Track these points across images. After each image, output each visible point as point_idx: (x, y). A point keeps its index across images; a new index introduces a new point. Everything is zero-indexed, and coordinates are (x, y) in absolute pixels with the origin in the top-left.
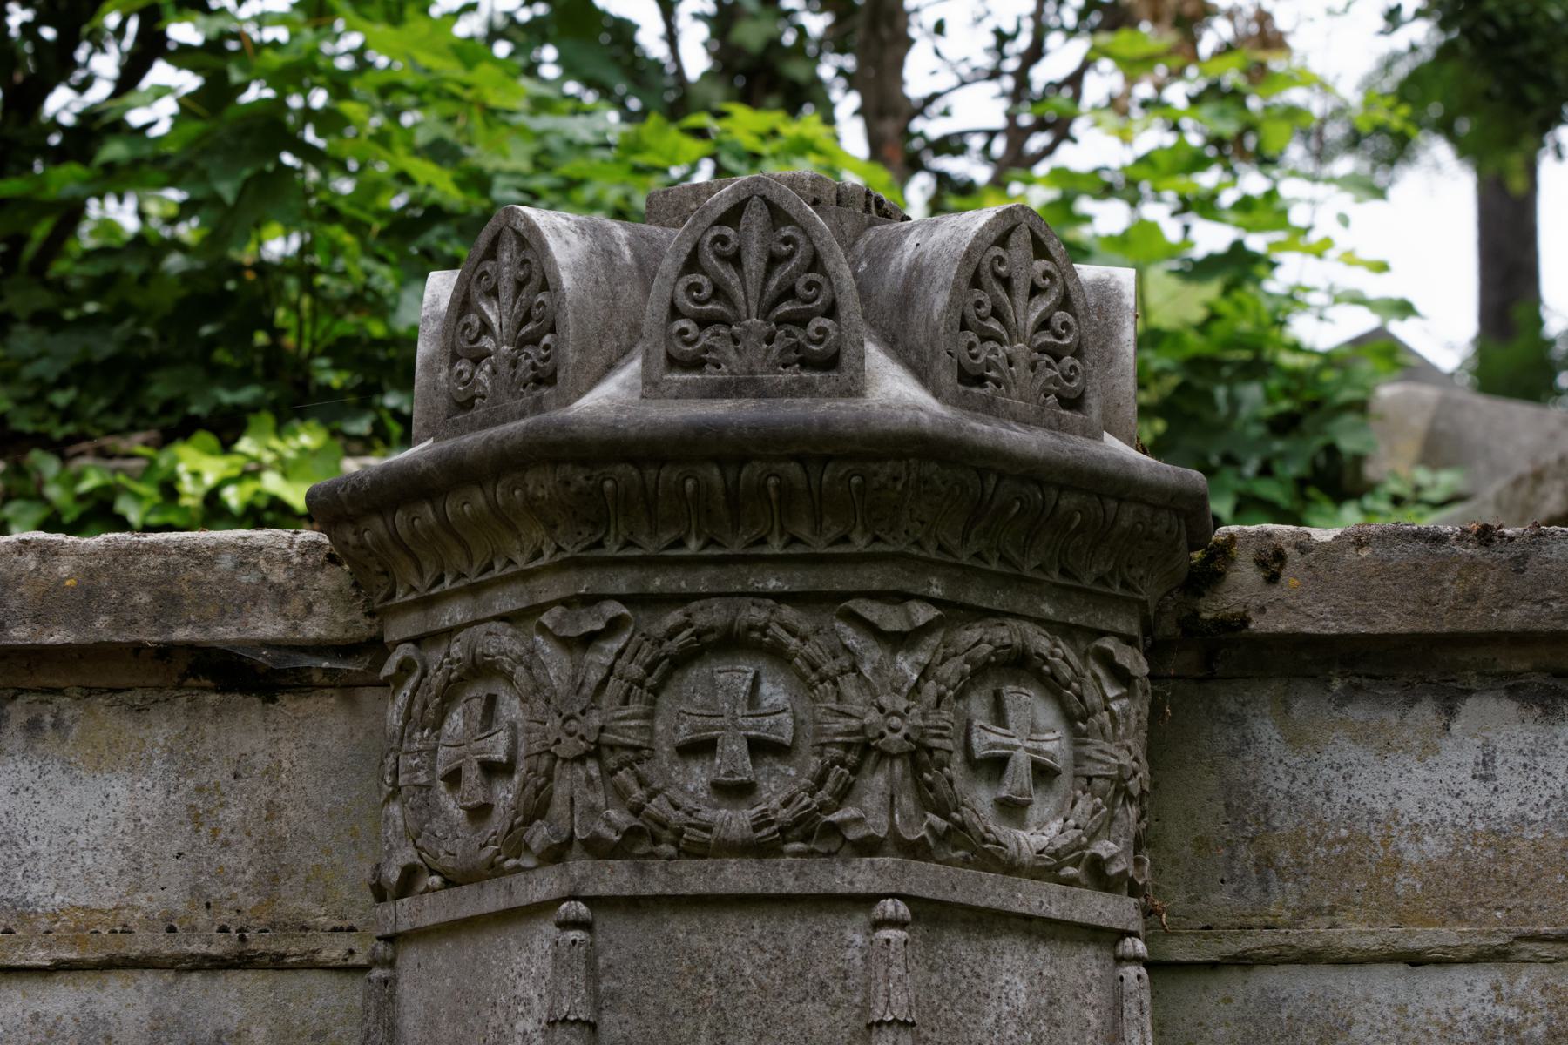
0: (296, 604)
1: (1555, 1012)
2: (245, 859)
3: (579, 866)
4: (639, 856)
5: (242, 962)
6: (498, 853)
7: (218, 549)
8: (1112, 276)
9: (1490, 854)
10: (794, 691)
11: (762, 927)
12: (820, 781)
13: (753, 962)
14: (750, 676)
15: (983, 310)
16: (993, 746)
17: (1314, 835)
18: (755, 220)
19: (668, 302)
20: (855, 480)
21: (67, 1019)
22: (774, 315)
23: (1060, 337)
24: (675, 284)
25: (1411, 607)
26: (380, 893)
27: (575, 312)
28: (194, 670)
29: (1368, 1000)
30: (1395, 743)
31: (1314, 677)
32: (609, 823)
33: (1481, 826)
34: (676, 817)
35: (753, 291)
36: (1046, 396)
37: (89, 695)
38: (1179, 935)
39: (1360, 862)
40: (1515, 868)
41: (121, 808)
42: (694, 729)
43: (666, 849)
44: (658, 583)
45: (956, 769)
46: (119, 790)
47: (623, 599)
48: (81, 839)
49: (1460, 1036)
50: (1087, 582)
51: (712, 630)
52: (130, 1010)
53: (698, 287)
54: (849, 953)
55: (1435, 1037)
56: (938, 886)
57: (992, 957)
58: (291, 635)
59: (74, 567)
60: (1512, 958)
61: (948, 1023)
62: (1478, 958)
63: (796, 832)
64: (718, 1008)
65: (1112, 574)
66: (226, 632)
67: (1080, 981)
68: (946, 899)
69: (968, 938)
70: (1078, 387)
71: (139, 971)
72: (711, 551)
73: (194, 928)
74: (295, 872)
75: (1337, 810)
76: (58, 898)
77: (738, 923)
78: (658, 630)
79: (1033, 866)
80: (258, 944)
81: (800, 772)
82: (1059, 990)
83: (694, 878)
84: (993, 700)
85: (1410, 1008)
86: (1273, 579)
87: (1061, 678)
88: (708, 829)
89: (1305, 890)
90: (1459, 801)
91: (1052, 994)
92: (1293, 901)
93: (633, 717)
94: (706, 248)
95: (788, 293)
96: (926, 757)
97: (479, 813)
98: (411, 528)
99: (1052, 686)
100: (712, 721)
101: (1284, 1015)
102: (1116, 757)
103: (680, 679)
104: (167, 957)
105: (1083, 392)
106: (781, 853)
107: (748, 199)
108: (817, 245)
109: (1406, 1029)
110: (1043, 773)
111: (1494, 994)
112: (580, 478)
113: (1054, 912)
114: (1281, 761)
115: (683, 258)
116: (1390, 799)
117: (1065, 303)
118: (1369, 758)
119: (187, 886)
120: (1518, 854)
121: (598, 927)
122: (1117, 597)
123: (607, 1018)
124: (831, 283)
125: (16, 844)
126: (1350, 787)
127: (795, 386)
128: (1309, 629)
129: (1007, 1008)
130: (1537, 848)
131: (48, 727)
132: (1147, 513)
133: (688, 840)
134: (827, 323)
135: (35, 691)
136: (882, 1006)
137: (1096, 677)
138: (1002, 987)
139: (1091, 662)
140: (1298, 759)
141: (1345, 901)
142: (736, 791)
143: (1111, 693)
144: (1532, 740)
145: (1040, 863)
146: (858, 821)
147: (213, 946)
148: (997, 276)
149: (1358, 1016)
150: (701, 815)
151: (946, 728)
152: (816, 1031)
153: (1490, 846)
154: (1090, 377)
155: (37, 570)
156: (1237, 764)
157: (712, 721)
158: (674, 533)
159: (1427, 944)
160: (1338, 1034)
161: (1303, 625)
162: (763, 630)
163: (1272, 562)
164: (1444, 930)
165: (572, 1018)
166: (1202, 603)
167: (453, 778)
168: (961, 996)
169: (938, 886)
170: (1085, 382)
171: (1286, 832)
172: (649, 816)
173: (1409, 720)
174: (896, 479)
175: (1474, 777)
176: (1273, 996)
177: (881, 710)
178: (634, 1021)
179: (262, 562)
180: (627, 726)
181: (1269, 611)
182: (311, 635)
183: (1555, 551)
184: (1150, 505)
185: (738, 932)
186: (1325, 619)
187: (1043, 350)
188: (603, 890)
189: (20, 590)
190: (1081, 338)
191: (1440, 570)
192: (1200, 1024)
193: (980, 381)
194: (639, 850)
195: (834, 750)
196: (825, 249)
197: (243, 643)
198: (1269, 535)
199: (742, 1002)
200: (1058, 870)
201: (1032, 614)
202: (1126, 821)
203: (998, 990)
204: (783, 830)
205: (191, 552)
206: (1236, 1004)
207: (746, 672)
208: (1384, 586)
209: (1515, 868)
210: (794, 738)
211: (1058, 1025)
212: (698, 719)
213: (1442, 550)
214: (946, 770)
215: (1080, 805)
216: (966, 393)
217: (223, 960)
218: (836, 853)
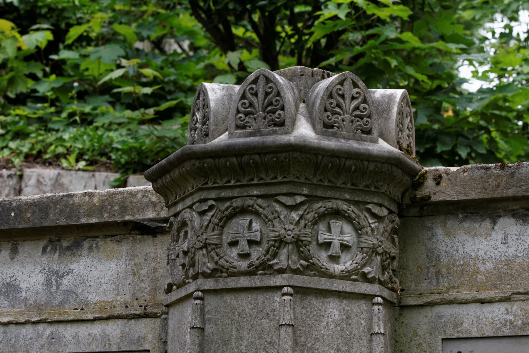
0: (159, 207)
1: (524, 317)
2: (147, 285)
3: (200, 281)
4: (217, 277)
5: (145, 316)
6: (184, 278)
7: (137, 192)
8: (395, 92)
9: (506, 267)
10: (262, 225)
11: (251, 297)
12: (267, 252)
13: (248, 308)
14: (248, 221)
15: (333, 105)
16: (325, 239)
17: (453, 264)
18: (261, 82)
19: (236, 108)
20: (274, 159)
21: (98, 334)
22: (266, 111)
23: (363, 112)
24: (238, 103)
25: (479, 190)
27: (214, 114)
28: (133, 229)
29: (468, 315)
30: (478, 233)
31: (454, 214)
32: (207, 267)
33: (503, 259)
34: (226, 265)
35: (260, 104)
36: (357, 131)
37: (106, 238)
38: (411, 297)
39: (467, 272)
40: (514, 271)
41: (114, 271)
42: (233, 238)
43: (225, 274)
44: (223, 194)
46: (113, 265)
47: (214, 199)
48: (103, 281)
49: (495, 325)
50: (361, 187)
51: (238, 207)
52: (115, 331)
53: (245, 104)
54: (275, 304)
55: (488, 326)
56: (304, 282)
57: (326, 304)
58: (157, 217)
59: (98, 200)
60: (512, 300)
61: (309, 325)
62: (501, 300)
63: (261, 268)
64: (238, 322)
65: (371, 184)
66: (139, 217)
67: (359, 311)
68: (307, 286)
69: (317, 298)
70: (369, 127)
71: (118, 320)
72: (239, 183)
73: (133, 306)
74: (161, 288)
75: (460, 256)
76: (96, 298)
77: (244, 296)
78: (223, 208)
79: (340, 276)
80: (149, 310)
81: (263, 249)
82: (351, 314)
83: (232, 283)
84: (328, 225)
85: (481, 317)
86: (438, 184)
87: (351, 217)
88: (235, 268)
89: (450, 281)
90: (497, 251)
91: (348, 315)
92: (446, 285)
93: (215, 235)
94: (247, 92)
95: (271, 104)
96: (300, 243)
98: (166, 182)
99: (349, 220)
100: (237, 235)
101: (443, 321)
102: (372, 241)
103: (230, 223)
104: (125, 315)
105: (371, 129)
106: (256, 274)
107: (259, 76)
108: (279, 88)
109: (479, 324)
110: (345, 247)
111: (506, 312)
112: (197, 163)
113: (348, 290)
114: (443, 241)
115: (241, 95)
116: (476, 251)
117: (365, 101)
118: (470, 239)
119: (131, 294)
120: (514, 267)
121: (205, 299)
122: (372, 192)
123: (207, 326)
124: (282, 100)
125: (85, 283)
126: (464, 248)
127: (271, 132)
128: (449, 199)
129: (331, 320)
130: (520, 265)
131: (94, 248)
132: (379, 165)
133: (230, 272)
134: (281, 112)
135: (91, 237)
136: (282, 319)
137: (365, 217)
138: (329, 313)
139: (364, 212)
140: (448, 240)
141: (462, 284)
142: (244, 256)
143: (371, 221)
144: (519, 231)
145: (342, 275)
146: (277, 263)
147: (137, 311)
148: (339, 94)
149: (465, 320)
150: (233, 264)
151: (307, 234)
152: (265, 328)
153: (506, 265)
154: (374, 124)
155: (88, 201)
156: (430, 242)
157: (237, 235)
158: (227, 179)
159: (485, 296)
160: (459, 326)
161: (447, 198)
162: (252, 206)
163: (438, 179)
164: (491, 292)
165: (195, 326)
166: (417, 192)
168: (314, 316)
169: (304, 282)
170: (372, 125)
171: (445, 263)
172: (219, 265)
173: (482, 226)
174: (286, 158)
175: (501, 243)
176: (440, 315)
177: (285, 229)
178: (215, 327)
179: (149, 195)
180: (212, 236)
181: (437, 194)
182: (163, 216)
183: (523, 170)
184: (380, 162)
185: (245, 299)
186: (453, 196)
187: (356, 116)
188: (206, 288)
189: (83, 207)
190: (370, 112)
191: (489, 178)
192: (418, 324)
193: (332, 127)
194: (217, 275)
195: (271, 242)
196: (281, 89)
197: (144, 220)
198: (437, 170)
199: (245, 320)
200: (350, 277)
201: (341, 198)
202: (376, 261)
203: (328, 314)
204: (256, 267)
205: (130, 193)
206: (429, 317)
207: (247, 220)
208: (472, 184)
209: (514, 271)
210: (261, 239)
211: (350, 325)
212: (233, 235)
213: (489, 172)
214: (307, 247)
215: (358, 256)
216: (325, 131)
217: (140, 315)
218: (273, 274)
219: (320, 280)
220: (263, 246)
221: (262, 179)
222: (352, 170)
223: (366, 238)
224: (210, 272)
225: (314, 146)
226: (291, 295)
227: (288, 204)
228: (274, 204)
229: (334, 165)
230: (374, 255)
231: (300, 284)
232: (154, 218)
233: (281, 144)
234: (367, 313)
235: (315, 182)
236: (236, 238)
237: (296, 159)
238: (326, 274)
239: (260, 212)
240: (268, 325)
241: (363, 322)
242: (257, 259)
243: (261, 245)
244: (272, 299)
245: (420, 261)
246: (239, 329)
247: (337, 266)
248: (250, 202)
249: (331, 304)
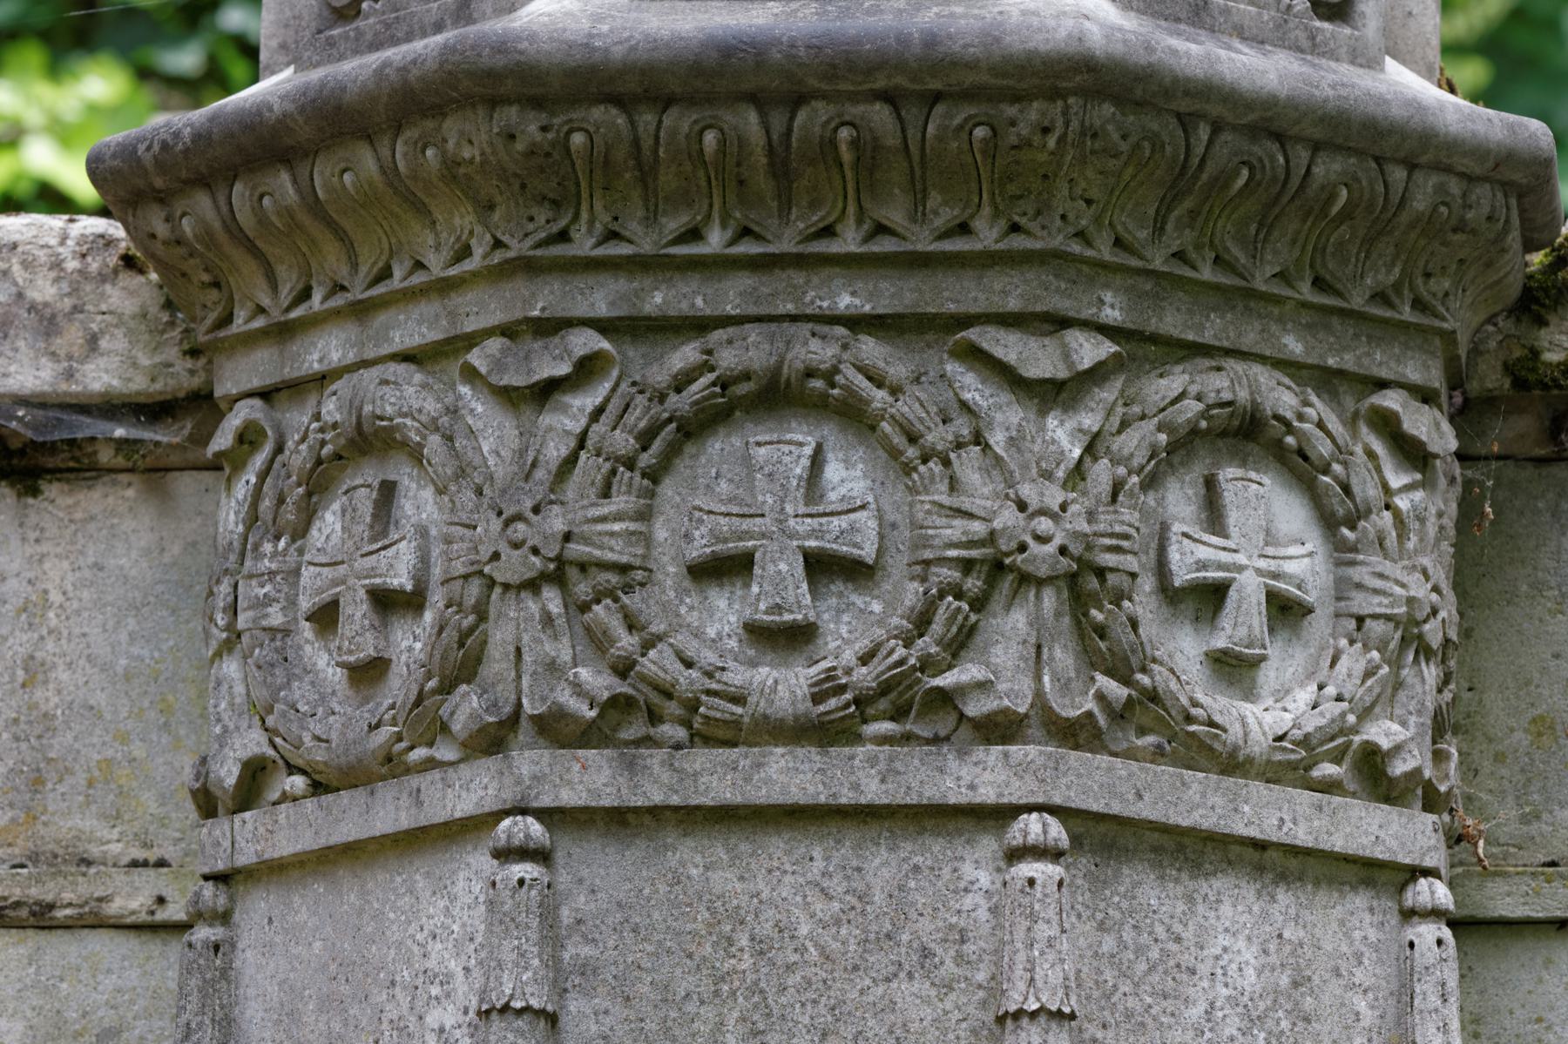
0: (72, 336)
4: (627, 744)
10: (880, 475)
11: (827, 859)
12: (922, 622)
14: (808, 451)
16: (1202, 565)
26: (207, 803)
32: (578, 688)
34: (688, 680)
45: (1144, 603)
47: (603, 327)
51: (746, 376)
54: (968, 901)
57: (1201, 909)
58: (64, 387)
61: (1129, 1015)
63: (883, 704)
64: (755, 989)
65: (1397, 287)
67: (1344, 948)
69: (1162, 878)
77: (788, 853)
78: (660, 376)
81: (890, 606)
88: (739, 700)
91: (1298, 969)
96: (1093, 583)
97: (367, 673)
100: (746, 524)
102: (1403, 586)
103: (695, 457)
106: (858, 739)
112: (533, 128)
113: (1302, 836)
121: (560, 857)
122: (1405, 326)
129: (1225, 992)
132: (1455, 187)
136: (1022, 986)
137: (1371, 455)
138: (1217, 958)
139: (1364, 430)
145: (1278, 757)
146: (983, 686)
150: (727, 677)
151: (1126, 537)
152: (914, 1027)
157: (746, 524)
162: (830, 376)
166: (1544, 336)
167: (326, 617)
172: (643, 678)
174: (1046, 131)
177: (1022, 506)
178: (618, 1010)
182: (96, 387)
185: (788, 867)
188: (569, 797)
192: (1539, 1020)
194: (627, 734)
199: (794, 979)
200: (1308, 769)
201: (1268, 353)
203: (1210, 962)
210: (880, 552)
212: (723, 520)
214: (1126, 603)
215: (1344, 664)
218: (947, 739)
219: (1184, 784)
220: (887, 587)
221: (881, 229)
222: (1335, 210)
223: (1379, 569)
224: (593, 714)
225: (1188, 72)
226: (1055, 855)
227: (1032, 372)
228: (953, 368)
229: (1258, 177)
230: (1411, 657)
231: (1096, 800)
232: (43, 394)
233: (1032, 55)
234: (1380, 961)
235: (1158, 264)
236: (741, 539)
237: (1095, 136)
238: (1211, 749)
239: (877, 405)
240: (927, 1013)
241: (1362, 1005)
242: (865, 659)
243: (877, 585)
244: (946, 872)
245: (1546, 692)
246: (761, 1026)
247: (1249, 706)
248: (820, 352)
249: (1226, 909)
